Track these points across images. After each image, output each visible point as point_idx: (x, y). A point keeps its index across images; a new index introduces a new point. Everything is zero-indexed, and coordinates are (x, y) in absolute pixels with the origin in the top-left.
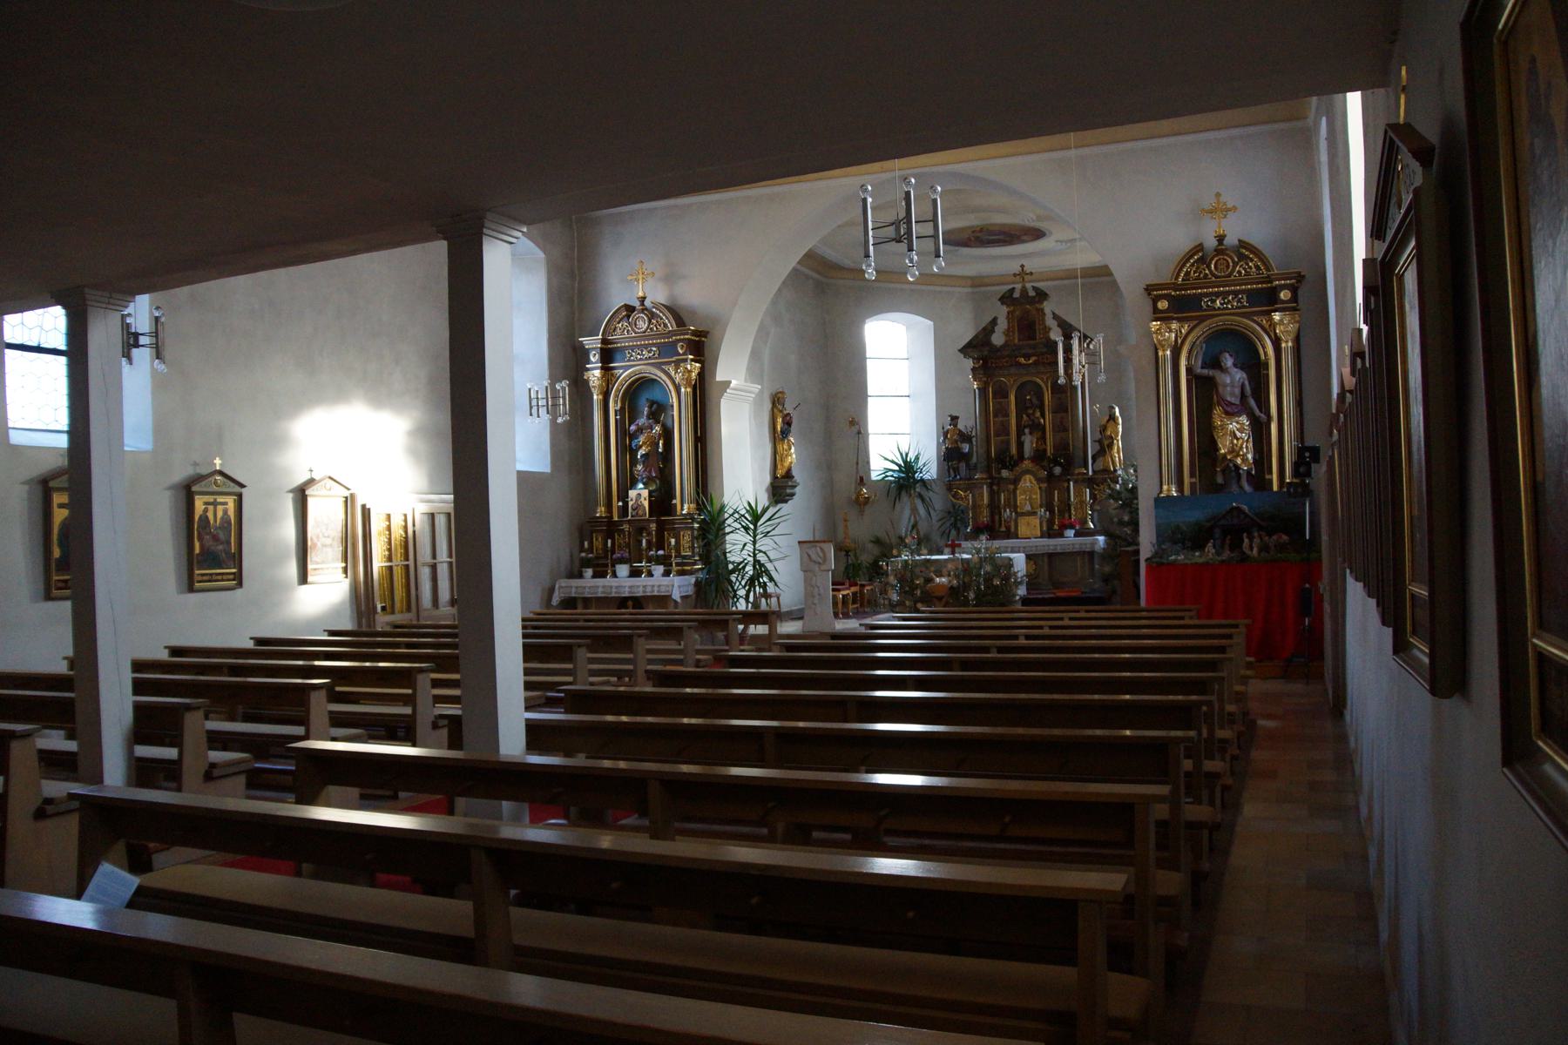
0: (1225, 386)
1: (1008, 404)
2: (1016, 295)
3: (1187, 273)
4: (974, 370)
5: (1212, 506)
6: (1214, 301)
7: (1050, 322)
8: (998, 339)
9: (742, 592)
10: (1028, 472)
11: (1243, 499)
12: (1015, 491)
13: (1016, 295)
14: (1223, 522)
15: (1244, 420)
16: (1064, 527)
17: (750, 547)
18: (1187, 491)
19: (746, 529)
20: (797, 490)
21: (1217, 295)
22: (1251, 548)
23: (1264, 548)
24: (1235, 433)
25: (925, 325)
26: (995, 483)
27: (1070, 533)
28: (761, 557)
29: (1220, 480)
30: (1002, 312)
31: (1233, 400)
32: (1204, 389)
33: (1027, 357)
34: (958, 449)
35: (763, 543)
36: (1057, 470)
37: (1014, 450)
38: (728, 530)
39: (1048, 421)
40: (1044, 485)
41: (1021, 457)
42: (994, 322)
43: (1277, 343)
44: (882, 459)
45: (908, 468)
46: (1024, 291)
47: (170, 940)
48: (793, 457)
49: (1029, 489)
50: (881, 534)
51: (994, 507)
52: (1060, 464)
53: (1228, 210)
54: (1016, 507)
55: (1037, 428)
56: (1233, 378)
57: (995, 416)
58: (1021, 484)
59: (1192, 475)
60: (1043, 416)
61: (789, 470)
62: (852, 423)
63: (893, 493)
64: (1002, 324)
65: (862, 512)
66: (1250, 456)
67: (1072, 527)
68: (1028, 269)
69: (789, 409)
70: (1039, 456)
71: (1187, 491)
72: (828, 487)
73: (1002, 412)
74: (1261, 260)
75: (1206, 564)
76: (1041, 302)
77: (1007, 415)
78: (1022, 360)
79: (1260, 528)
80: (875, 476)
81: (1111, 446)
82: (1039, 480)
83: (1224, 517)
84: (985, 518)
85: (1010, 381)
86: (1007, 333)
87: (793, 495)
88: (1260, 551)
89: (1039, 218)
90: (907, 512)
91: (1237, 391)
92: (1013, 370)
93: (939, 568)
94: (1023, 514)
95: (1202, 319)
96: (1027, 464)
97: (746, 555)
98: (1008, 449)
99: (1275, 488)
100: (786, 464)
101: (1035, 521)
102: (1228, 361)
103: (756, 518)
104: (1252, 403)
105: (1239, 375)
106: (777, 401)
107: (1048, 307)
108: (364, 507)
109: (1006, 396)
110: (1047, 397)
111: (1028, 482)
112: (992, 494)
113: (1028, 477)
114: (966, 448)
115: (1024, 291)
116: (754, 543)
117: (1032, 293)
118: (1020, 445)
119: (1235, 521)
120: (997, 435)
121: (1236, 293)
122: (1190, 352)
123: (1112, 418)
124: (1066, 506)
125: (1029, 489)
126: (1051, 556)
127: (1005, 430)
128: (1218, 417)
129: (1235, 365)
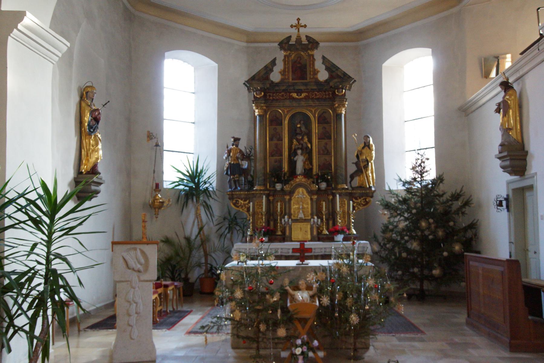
2: (293, 41)
7: (319, 65)
8: (276, 76)
9: (21, 321)
10: (300, 185)
12: (290, 200)
13: (293, 41)
16: (335, 232)
17: (41, 250)
19: (37, 223)
20: (102, 188)
25: (210, 65)
26: (271, 194)
27: (340, 237)
28: (58, 265)
30: (280, 55)
33: (299, 92)
34: (238, 165)
35: (64, 245)
37: (286, 167)
38: (8, 222)
40: (315, 197)
41: (293, 173)
44: (173, 171)
45: (195, 176)
46: (299, 39)
48: (100, 154)
49: (301, 201)
50: (171, 235)
51: (271, 215)
52: (326, 181)
57: (271, 139)
58: (296, 195)
60: (310, 141)
61: (95, 166)
62: (150, 136)
63: (182, 200)
64: (279, 67)
65: (157, 215)
67: (341, 232)
68: (302, 22)
69: (97, 104)
70: (308, 173)
72: (128, 190)
73: (276, 137)
76: (312, 49)
77: (281, 139)
78: (295, 95)
80: (167, 185)
81: (366, 167)
82: (311, 193)
84: (262, 222)
86: (283, 73)
87: (98, 192)
90: (192, 216)
92: (287, 103)
93: (295, 278)
96: (300, 179)
97: (36, 261)
98: (281, 167)
100: (92, 160)
101: (307, 227)
103: (54, 207)
106: (85, 95)
107: (318, 54)
109: (281, 124)
110: (315, 128)
111: (301, 192)
112: (268, 202)
113: (301, 190)
115: (299, 39)
116: (49, 243)
117: (304, 41)
118: (292, 164)
120: (272, 155)
123: (367, 145)
124: (332, 215)
125: (301, 201)
127: (277, 151)
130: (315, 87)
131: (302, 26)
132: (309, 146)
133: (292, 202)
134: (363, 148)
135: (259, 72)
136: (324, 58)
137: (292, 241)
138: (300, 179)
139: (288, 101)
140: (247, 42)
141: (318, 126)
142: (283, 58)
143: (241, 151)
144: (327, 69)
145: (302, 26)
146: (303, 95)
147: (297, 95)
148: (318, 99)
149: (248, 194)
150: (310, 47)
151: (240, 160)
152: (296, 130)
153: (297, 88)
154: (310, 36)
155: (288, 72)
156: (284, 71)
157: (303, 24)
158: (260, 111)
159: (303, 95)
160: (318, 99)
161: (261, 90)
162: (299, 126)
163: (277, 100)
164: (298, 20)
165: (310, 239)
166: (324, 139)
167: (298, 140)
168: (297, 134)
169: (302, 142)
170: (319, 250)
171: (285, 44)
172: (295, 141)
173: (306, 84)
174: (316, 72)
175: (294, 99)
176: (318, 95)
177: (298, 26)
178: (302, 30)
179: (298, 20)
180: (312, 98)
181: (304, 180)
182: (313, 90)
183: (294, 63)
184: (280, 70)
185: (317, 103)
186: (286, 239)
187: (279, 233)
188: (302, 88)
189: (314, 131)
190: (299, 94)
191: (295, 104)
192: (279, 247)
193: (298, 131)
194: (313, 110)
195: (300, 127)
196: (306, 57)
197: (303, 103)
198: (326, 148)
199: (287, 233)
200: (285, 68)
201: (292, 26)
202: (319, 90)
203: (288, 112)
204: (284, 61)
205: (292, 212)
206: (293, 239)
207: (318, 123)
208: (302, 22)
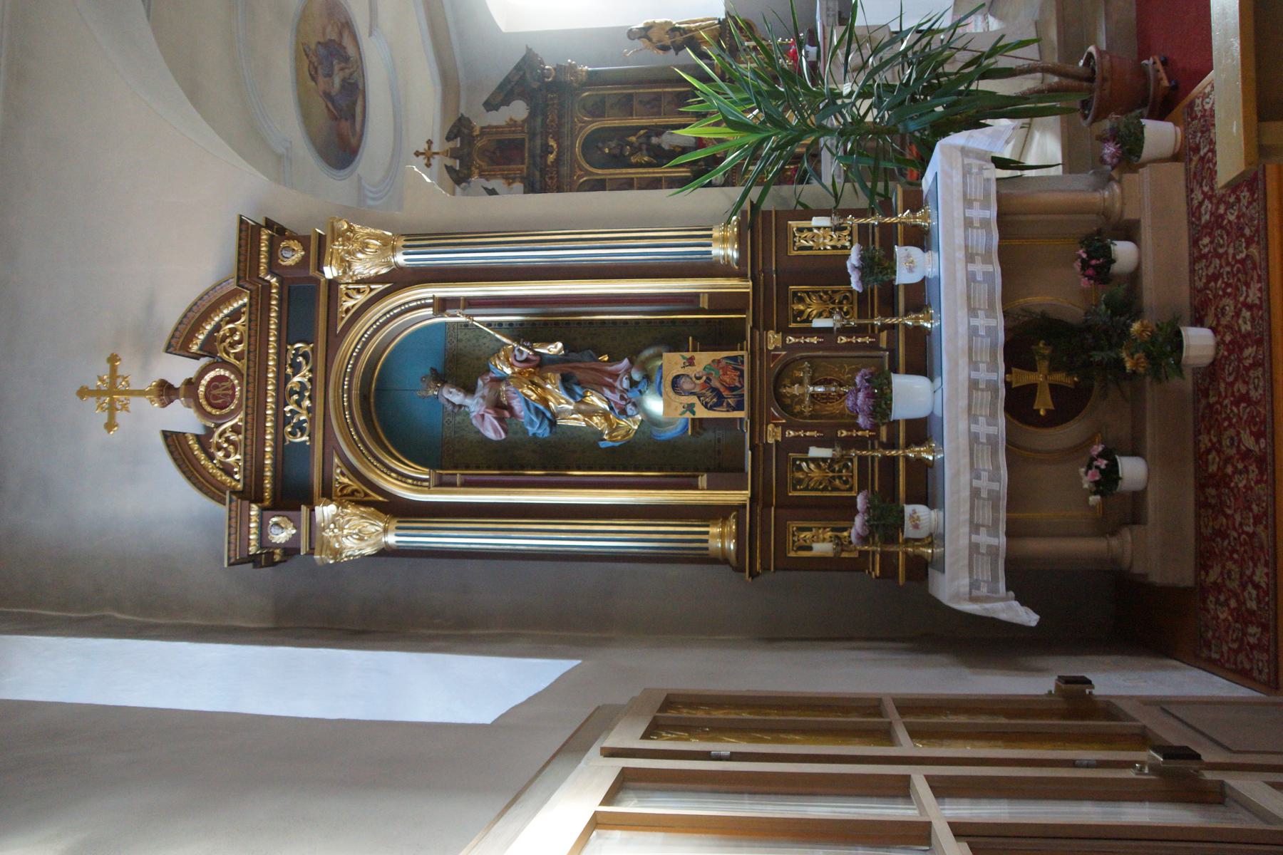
2: (457, 164)
7: (499, 118)
13: (457, 164)
33: (547, 150)
46: (453, 154)
60: (635, 130)
78: (551, 157)
92: (565, 170)
108: (166, 435)
115: (453, 154)
134: (650, 40)
146: (552, 143)
164: (417, 154)
174: (513, 123)
175: (557, 160)
179: (417, 154)
191: (567, 157)
193: (617, 151)
194: (579, 173)
197: (567, 143)
198: (648, 102)
201: (428, 165)
208: (423, 147)
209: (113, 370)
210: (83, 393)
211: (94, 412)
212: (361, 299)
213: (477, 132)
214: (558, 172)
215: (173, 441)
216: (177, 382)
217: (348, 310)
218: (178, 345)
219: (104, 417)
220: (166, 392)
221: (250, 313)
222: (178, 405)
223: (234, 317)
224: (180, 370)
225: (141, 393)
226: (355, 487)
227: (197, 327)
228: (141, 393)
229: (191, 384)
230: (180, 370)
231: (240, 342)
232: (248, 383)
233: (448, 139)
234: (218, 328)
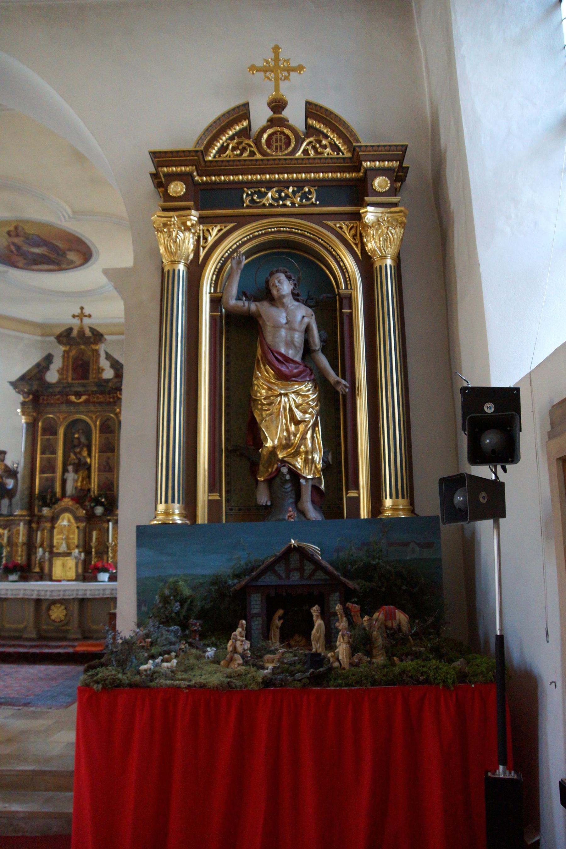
0: (277, 327)
1: (56, 440)
2: (75, 333)
3: (223, 149)
4: (23, 404)
5: (257, 544)
6: (262, 195)
7: (104, 363)
8: (52, 376)
10: (66, 510)
11: (306, 531)
12: (53, 528)
13: (75, 333)
14: (269, 580)
15: (307, 388)
18: (202, 516)
21: (270, 185)
22: (330, 644)
23: (362, 644)
24: (290, 416)
26: (34, 521)
29: (263, 498)
30: (59, 351)
31: (290, 353)
32: (240, 332)
33: (78, 395)
36: (99, 510)
37: (58, 489)
39: (94, 461)
40: (83, 525)
42: (49, 359)
43: (366, 263)
46: (81, 332)
47: (452, 474)
51: (30, 546)
52: (102, 504)
53: (290, 70)
54: (51, 546)
55: (82, 467)
56: (290, 321)
59: (213, 487)
60: (90, 455)
64: (57, 364)
66: (317, 457)
71: (202, 516)
73: (49, 448)
74: (341, 135)
75: (226, 691)
77: (54, 452)
78: (73, 398)
79: (347, 595)
82: (77, 519)
83: (270, 568)
85: (60, 417)
86: (61, 371)
88: (354, 649)
89: (77, 214)
91: (298, 338)
92: (64, 408)
94: (59, 555)
95: (241, 221)
96: (67, 502)
98: (52, 486)
99: (364, 514)
101: (71, 562)
102: (285, 287)
104: (323, 361)
105: (302, 314)
107: (102, 348)
110: (96, 437)
111: (65, 520)
112: (31, 534)
113: (67, 515)
114: (10, 483)
115: (81, 332)
117: (88, 333)
118: (64, 482)
119: (295, 577)
121: (299, 185)
122: (219, 272)
125: (66, 527)
126: (82, 602)
127: (49, 467)
128: (263, 383)
129: (295, 296)
130: (95, 389)
131: (86, 316)
132: (88, 460)
133: (55, 531)
135: (30, 371)
136: (106, 353)
137: (51, 580)
138: (67, 502)
139: (64, 405)
140: (43, 335)
141: (100, 437)
142: (62, 354)
143: (6, 466)
144: (112, 366)
145: (86, 316)
146: (84, 398)
147: (76, 398)
148: (100, 403)
149: (8, 521)
150: (92, 340)
151: (4, 479)
152: (73, 441)
153: (74, 389)
154: (93, 327)
155: (67, 372)
156: (62, 369)
157: (87, 314)
158: (28, 417)
159: (84, 398)
160: (100, 403)
161: (28, 393)
162: (76, 436)
163: (52, 404)
164: (82, 308)
165: (74, 578)
166: (106, 452)
167: (75, 454)
168: (75, 446)
169: (79, 456)
170: (70, 593)
171: (65, 337)
172: (72, 456)
173: (84, 386)
174: (100, 370)
176: (101, 398)
177: (82, 315)
178: (86, 321)
179: (82, 308)
180: (94, 402)
181: (70, 503)
182: (94, 393)
183: (76, 359)
184: (58, 369)
185: (99, 408)
186: (44, 577)
187: (37, 570)
188: (80, 389)
189: (94, 442)
190: (78, 397)
191: (72, 409)
192: (21, 587)
193: (76, 442)
194: (94, 417)
195: (78, 438)
196: (90, 353)
197: (82, 408)
198: (108, 463)
199: (46, 570)
200: (63, 366)
201: (74, 316)
202: (102, 393)
203: (97, 418)
204: (63, 357)
205: (55, 544)
206: (54, 578)
207: (100, 432)
208: (86, 312)
209: (294, 70)
210: (276, 49)
211: (262, 56)
212: (349, 237)
213: (94, 347)
214: (62, 403)
215: (242, 112)
216: (286, 113)
217: (341, 228)
218: (313, 110)
219: (260, 63)
220: (278, 105)
221: (337, 158)
222: (269, 113)
223: (335, 147)
224: (295, 115)
225: (277, 88)
226: (210, 239)
227: (327, 123)
228: (277, 88)
229: (283, 122)
230: (295, 115)
231: (316, 152)
232: (285, 159)
233: (92, 330)
234: (326, 137)
